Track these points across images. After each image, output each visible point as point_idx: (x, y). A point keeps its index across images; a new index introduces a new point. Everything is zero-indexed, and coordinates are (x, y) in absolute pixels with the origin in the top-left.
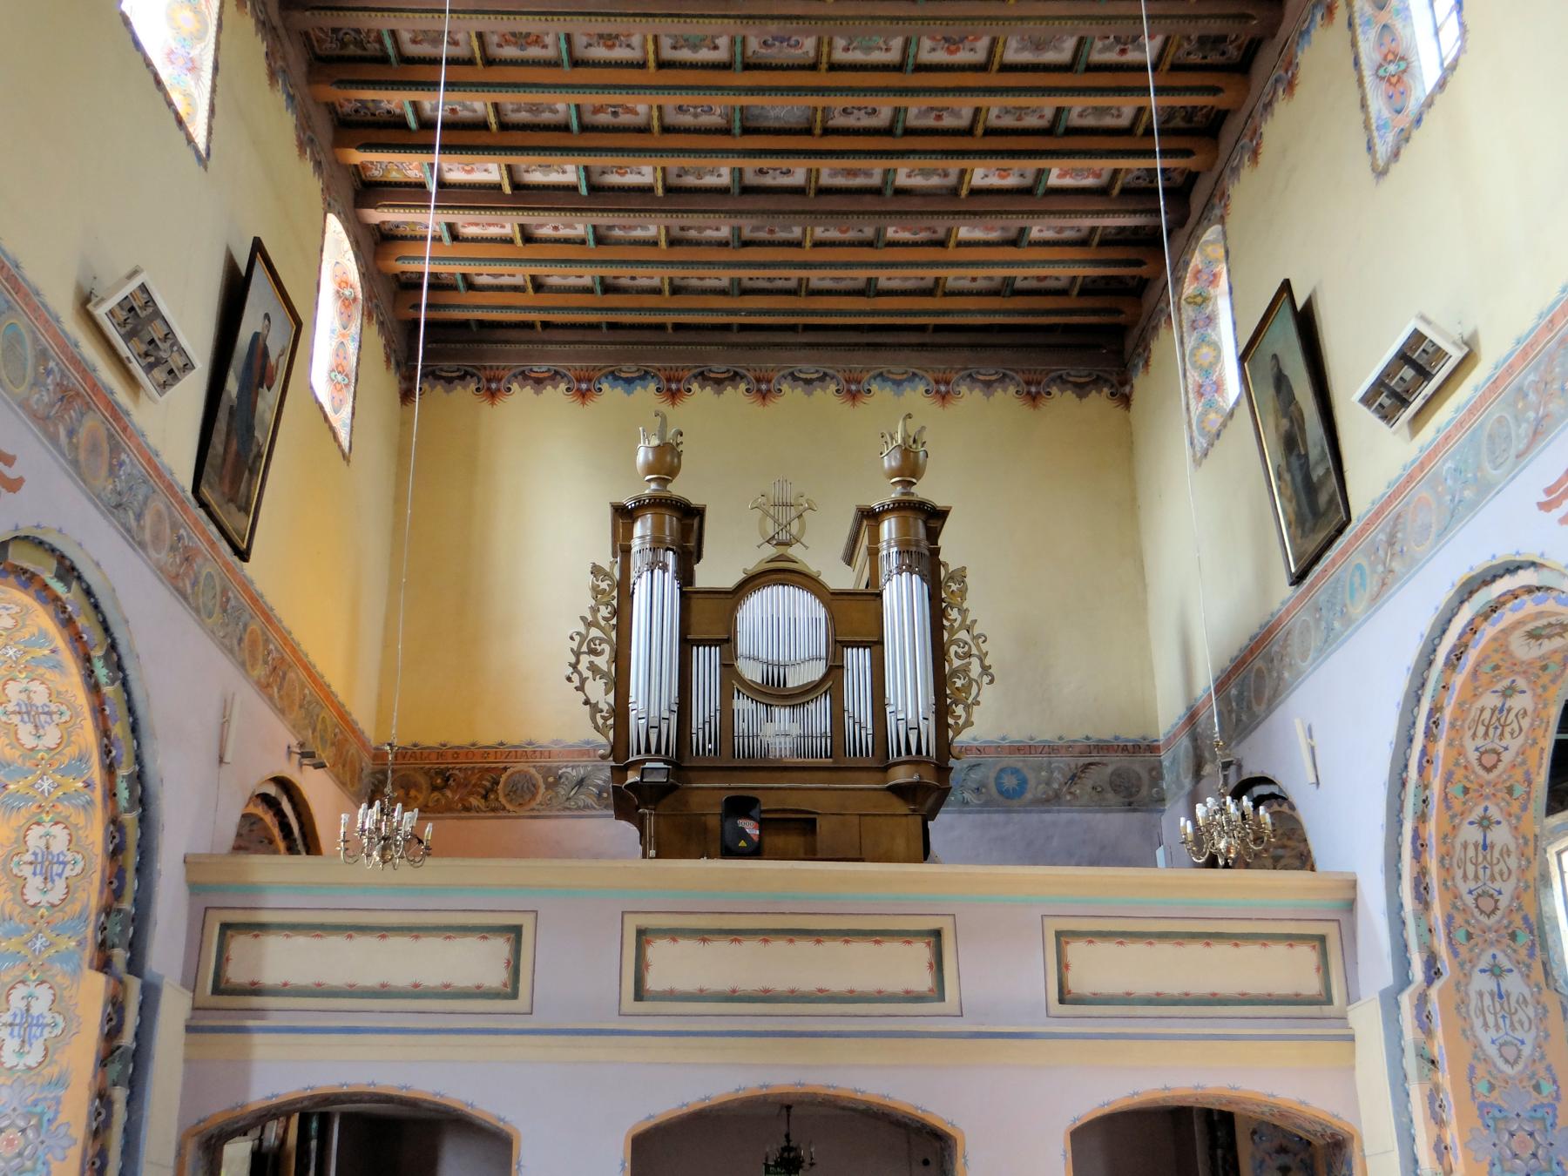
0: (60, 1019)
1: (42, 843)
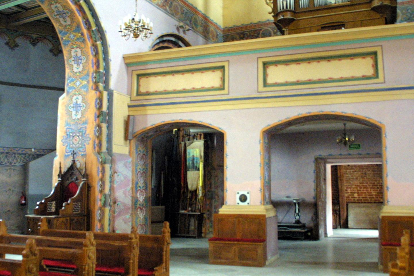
0: (84, 104)
1: (75, 54)
